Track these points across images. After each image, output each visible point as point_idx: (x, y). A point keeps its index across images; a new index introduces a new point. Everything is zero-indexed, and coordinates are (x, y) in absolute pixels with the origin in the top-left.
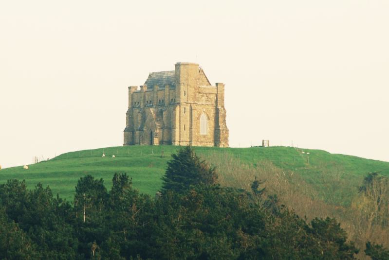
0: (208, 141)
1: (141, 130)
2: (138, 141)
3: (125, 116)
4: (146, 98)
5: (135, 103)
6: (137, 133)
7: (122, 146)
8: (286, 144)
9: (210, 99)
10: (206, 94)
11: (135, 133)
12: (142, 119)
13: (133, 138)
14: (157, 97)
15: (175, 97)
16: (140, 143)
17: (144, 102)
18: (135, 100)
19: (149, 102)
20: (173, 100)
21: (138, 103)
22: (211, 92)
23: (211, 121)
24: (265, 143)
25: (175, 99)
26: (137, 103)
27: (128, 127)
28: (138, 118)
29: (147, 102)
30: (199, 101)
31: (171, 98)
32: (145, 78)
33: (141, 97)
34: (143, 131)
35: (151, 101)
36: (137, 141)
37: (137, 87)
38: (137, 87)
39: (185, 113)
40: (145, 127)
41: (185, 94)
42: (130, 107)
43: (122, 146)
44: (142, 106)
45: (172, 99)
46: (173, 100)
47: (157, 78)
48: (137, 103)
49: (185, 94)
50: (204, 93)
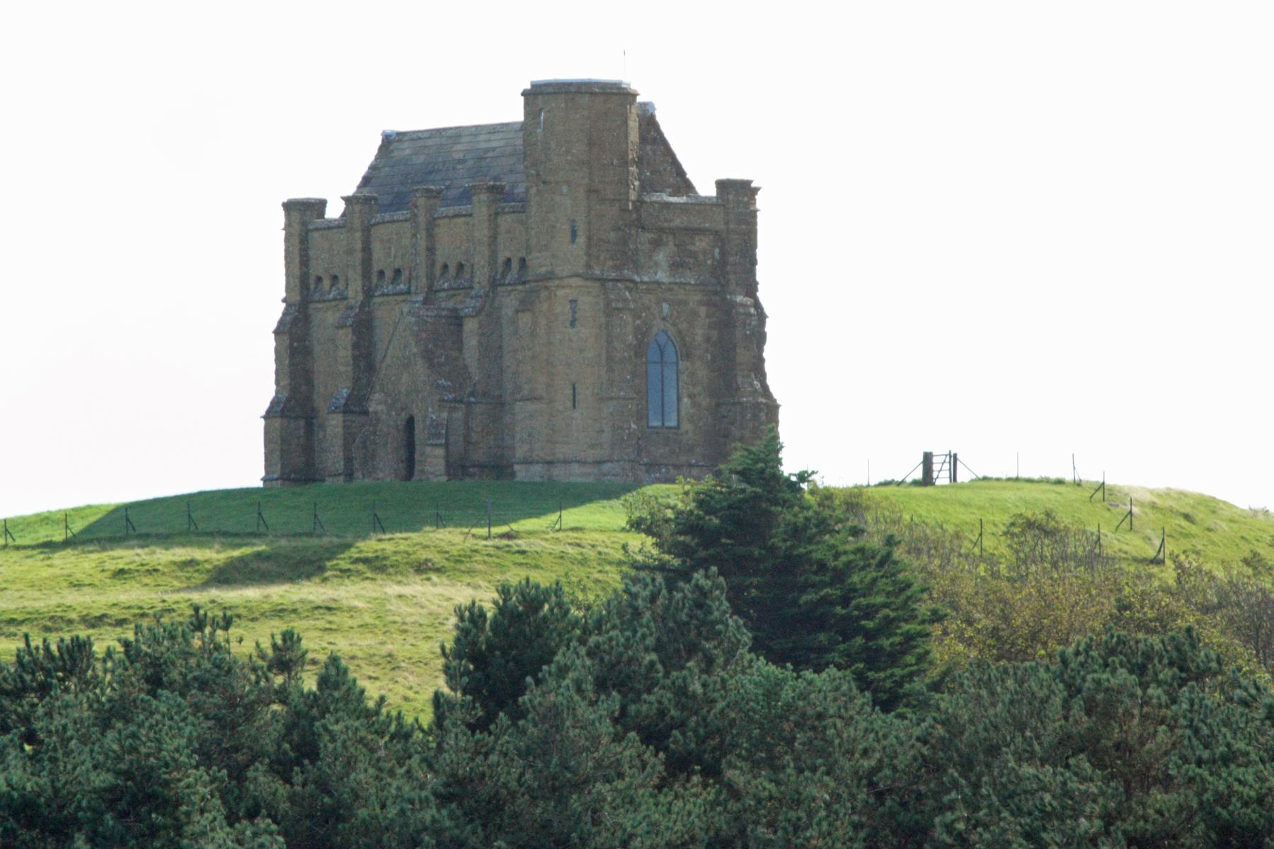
0: (683, 459)
1: (355, 406)
2: (340, 466)
3: (271, 343)
4: (375, 256)
5: (319, 279)
6: (334, 425)
7: (260, 484)
8: (273, 356)
9: (693, 255)
10: (673, 231)
11: (322, 427)
12: (778, 451)
13: (309, 449)
14: (431, 250)
15: (529, 249)
16: (350, 476)
17: (366, 275)
18: (316, 269)
19: (389, 274)
20: (515, 265)
21: (335, 278)
22: (696, 222)
23: (698, 363)
24: (936, 467)
25: (523, 261)
26: (326, 283)
27: (286, 394)
28: (88, 511)
29: (381, 273)
30: (637, 267)
31: (501, 259)
32: (365, 155)
33: (350, 252)
34: (366, 413)
35: (398, 272)
36: (333, 458)
37: (321, 204)
38: (321, 204)
39: (573, 324)
40: (377, 396)
41: (574, 234)
42: (297, 298)
43: (260, 484)
44: (355, 291)
45: (508, 261)
46: (515, 265)
47: (421, 159)
48: (326, 283)
49: (574, 234)
50: (662, 230)
